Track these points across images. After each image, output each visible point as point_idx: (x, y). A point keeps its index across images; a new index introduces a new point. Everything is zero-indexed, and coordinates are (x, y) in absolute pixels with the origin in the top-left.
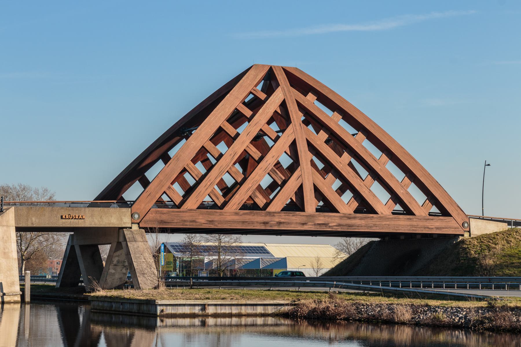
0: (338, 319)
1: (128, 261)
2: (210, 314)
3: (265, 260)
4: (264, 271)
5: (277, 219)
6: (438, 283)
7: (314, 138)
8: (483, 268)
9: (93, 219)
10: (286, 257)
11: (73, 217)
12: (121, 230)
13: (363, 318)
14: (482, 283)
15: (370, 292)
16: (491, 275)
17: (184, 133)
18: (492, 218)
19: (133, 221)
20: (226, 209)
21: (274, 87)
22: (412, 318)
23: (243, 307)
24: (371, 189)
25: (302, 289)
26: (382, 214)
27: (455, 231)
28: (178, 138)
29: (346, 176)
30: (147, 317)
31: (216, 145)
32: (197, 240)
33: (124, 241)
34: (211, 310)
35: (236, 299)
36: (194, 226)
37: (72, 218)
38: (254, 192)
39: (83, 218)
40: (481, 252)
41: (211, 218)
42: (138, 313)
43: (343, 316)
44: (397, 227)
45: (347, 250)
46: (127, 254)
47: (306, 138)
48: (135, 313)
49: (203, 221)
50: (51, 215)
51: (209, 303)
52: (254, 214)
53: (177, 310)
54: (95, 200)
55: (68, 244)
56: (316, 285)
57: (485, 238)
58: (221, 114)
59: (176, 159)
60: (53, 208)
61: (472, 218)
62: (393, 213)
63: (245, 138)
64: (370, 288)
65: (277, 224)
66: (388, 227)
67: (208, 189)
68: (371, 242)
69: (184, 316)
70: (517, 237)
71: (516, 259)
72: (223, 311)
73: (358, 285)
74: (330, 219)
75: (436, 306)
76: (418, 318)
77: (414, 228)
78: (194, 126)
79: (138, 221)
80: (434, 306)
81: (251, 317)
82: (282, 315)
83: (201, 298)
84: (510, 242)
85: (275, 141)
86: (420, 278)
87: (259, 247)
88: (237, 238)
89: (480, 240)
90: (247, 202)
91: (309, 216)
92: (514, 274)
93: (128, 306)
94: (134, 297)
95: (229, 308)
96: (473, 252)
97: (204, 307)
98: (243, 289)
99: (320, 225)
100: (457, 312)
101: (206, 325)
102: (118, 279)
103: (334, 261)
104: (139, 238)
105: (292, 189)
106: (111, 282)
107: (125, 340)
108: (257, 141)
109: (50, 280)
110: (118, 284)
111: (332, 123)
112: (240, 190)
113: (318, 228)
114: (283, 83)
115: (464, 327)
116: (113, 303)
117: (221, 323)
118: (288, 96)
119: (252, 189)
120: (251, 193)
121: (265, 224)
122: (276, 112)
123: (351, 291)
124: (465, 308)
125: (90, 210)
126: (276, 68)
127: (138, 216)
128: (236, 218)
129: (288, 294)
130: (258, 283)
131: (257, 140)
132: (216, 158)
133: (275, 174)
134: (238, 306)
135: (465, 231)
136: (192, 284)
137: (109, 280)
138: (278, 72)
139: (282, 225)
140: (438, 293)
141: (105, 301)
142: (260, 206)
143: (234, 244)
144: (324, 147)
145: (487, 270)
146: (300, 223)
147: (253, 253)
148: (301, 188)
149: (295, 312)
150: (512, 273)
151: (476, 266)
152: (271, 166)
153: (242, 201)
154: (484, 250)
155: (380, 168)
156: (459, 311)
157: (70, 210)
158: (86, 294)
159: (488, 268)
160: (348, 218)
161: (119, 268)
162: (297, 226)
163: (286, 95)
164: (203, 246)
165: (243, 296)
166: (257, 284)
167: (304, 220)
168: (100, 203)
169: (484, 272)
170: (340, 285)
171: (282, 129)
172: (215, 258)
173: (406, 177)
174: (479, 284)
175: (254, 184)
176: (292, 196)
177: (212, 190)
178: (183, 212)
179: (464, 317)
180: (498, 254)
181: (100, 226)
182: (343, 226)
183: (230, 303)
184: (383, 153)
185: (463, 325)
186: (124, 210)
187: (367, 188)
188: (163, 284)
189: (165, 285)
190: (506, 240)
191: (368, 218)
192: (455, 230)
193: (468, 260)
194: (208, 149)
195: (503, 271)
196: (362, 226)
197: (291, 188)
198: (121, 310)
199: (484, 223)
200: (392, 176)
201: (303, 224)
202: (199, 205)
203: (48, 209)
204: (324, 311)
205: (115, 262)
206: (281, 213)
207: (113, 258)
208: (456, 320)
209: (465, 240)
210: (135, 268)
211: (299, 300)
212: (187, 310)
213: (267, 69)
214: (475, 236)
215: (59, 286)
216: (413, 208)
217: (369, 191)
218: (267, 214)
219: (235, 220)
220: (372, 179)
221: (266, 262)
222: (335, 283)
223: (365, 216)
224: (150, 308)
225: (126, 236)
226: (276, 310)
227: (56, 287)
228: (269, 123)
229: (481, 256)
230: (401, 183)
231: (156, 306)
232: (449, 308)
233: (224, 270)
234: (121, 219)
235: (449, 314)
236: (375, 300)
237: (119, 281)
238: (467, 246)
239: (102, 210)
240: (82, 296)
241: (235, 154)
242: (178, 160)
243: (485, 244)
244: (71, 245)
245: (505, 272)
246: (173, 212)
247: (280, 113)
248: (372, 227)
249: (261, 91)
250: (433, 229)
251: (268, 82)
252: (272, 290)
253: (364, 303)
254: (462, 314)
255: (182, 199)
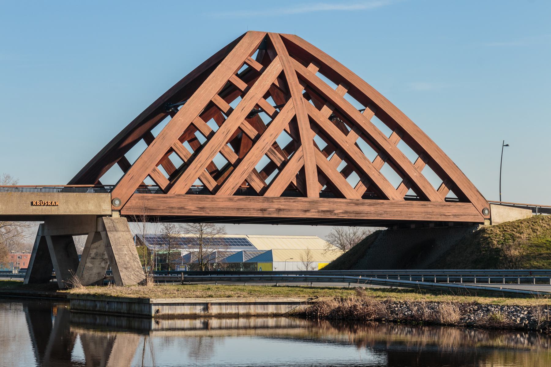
0: (368, 320)
1: (108, 254)
2: (213, 315)
3: (248, 253)
4: (246, 265)
5: (276, 206)
6: (457, 277)
7: (317, 114)
8: (508, 260)
9: (68, 205)
10: (271, 250)
11: (45, 204)
12: (100, 219)
13: (398, 319)
14: (521, 277)
15: (398, 288)
16: (517, 268)
17: (169, 110)
18: (514, 204)
19: (113, 208)
20: (219, 194)
21: (271, 57)
22: (461, 319)
23: (252, 307)
24: (381, 171)
25: (315, 284)
26: (393, 199)
27: (474, 218)
28: (163, 114)
29: (353, 157)
30: (139, 318)
31: (206, 122)
32: (175, 231)
33: (103, 231)
34: (214, 310)
35: (244, 297)
36: (182, 214)
37: (44, 205)
38: (250, 175)
39: (56, 205)
40: (505, 242)
41: (202, 204)
42: (128, 313)
43: (373, 317)
44: (409, 215)
45: (339, 242)
46: (106, 245)
47: (308, 115)
48: (124, 313)
49: (193, 208)
50: (20, 202)
51: (212, 302)
52: (250, 200)
53: (174, 310)
54: (69, 184)
55: (38, 235)
56: (346, 280)
57: (508, 226)
58: (212, 86)
59: (162, 137)
60: (22, 194)
61: (492, 204)
62: (406, 199)
63: (240, 113)
64: (399, 283)
65: (276, 211)
66: (400, 214)
67: (198, 171)
68: (377, 231)
69: (183, 317)
70: (544, 225)
71: (544, 249)
72: (229, 311)
73: (384, 280)
74: (335, 205)
75: (487, 304)
76: (469, 319)
77: (428, 216)
78: (181, 101)
79: (119, 208)
80: (486, 304)
81: (261, 318)
82: (297, 315)
83: (203, 296)
84: (536, 231)
85: (273, 117)
86: (447, 271)
87: (240, 239)
88: (220, 229)
89: (503, 228)
90: (242, 186)
91: (312, 202)
92: (544, 267)
93: (116, 306)
94: (123, 294)
95: (235, 308)
96: (495, 242)
97: (206, 306)
98: (172, 284)
99: (324, 212)
100: (516, 311)
101: (209, 327)
102: (96, 274)
103: (325, 254)
104: (120, 227)
105: (293, 171)
106: (88, 278)
107: (105, 344)
108: (251, 118)
109: (16, 276)
110: (96, 279)
111: (336, 97)
112: (234, 173)
113: (322, 216)
114: (281, 52)
115: (530, 330)
116: (97, 302)
117: (226, 325)
118: (287, 66)
119: (247, 172)
120: (246, 176)
121: (262, 211)
122: (273, 84)
123: (375, 286)
124: (525, 307)
125: (64, 195)
126: (273, 35)
127: (119, 203)
128: (230, 204)
129: (302, 291)
130: (262, 278)
131: (251, 117)
132: (207, 136)
133: (273, 155)
134: (246, 305)
135: (485, 219)
136: (183, 279)
137: (86, 275)
138: (275, 40)
139: (281, 212)
140: (484, 288)
141: (88, 300)
142: (256, 191)
143: (217, 236)
144: (328, 124)
145: (513, 262)
146: (302, 210)
147: (238, 245)
148: (303, 170)
149: (314, 311)
150: (541, 265)
151: (500, 258)
152: (269, 146)
153: (237, 185)
154: (507, 240)
155: (390, 148)
156: (518, 310)
157: (41, 196)
158: (60, 291)
159: (514, 260)
160: (355, 204)
161: (97, 262)
162: (299, 214)
163: (285, 66)
164: (184, 238)
165: (250, 293)
166: (261, 279)
167: (306, 206)
168: (75, 187)
169: (510, 264)
170: (367, 280)
171: (278, 105)
172: (196, 251)
173: (419, 158)
174: (460, 278)
175: (250, 166)
176: (293, 180)
177: (203, 173)
178: (170, 197)
179: (526, 318)
180: (524, 244)
181: (76, 214)
182: (350, 213)
183: (237, 302)
184: (393, 131)
185: (529, 328)
186: (103, 195)
187: (377, 170)
188: (151, 280)
189: (154, 281)
190: (531, 228)
191: (378, 204)
192: (474, 218)
193: (490, 251)
194: (198, 126)
195: (530, 263)
196: (371, 214)
197: (292, 171)
198: (107, 310)
199: (506, 209)
200: (404, 157)
201: (306, 211)
202: (188, 190)
203: (16, 194)
204: (350, 311)
205: (93, 255)
206: (281, 198)
207: (90, 250)
208: (518, 321)
209: (486, 229)
210: (117, 261)
211: (317, 297)
212: (186, 310)
213: (262, 37)
214: (497, 224)
215: (27, 282)
216: (428, 193)
217: (379, 174)
218: (265, 200)
219: (228, 207)
220: (382, 161)
221: (250, 255)
222: (360, 277)
223: (374, 202)
224: (143, 307)
225: (105, 225)
226: (290, 309)
227: (24, 284)
228: (265, 97)
229: (505, 247)
230: (414, 164)
231: (150, 305)
232: (505, 307)
233: (206, 264)
234: (100, 206)
235: (507, 313)
236: (410, 297)
237: (97, 277)
238: (488, 235)
239: (77, 196)
240: (55, 293)
241: (229, 131)
242: (164, 139)
243: (508, 232)
244: (42, 236)
245: (534, 264)
246: (159, 197)
247: (279, 86)
248: (383, 214)
249: (256, 60)
250: (450, 216)
251: (264, 51)
252: (279, 286)
253: (396, 300)
254: (523, 314)
255: (168, 183)
